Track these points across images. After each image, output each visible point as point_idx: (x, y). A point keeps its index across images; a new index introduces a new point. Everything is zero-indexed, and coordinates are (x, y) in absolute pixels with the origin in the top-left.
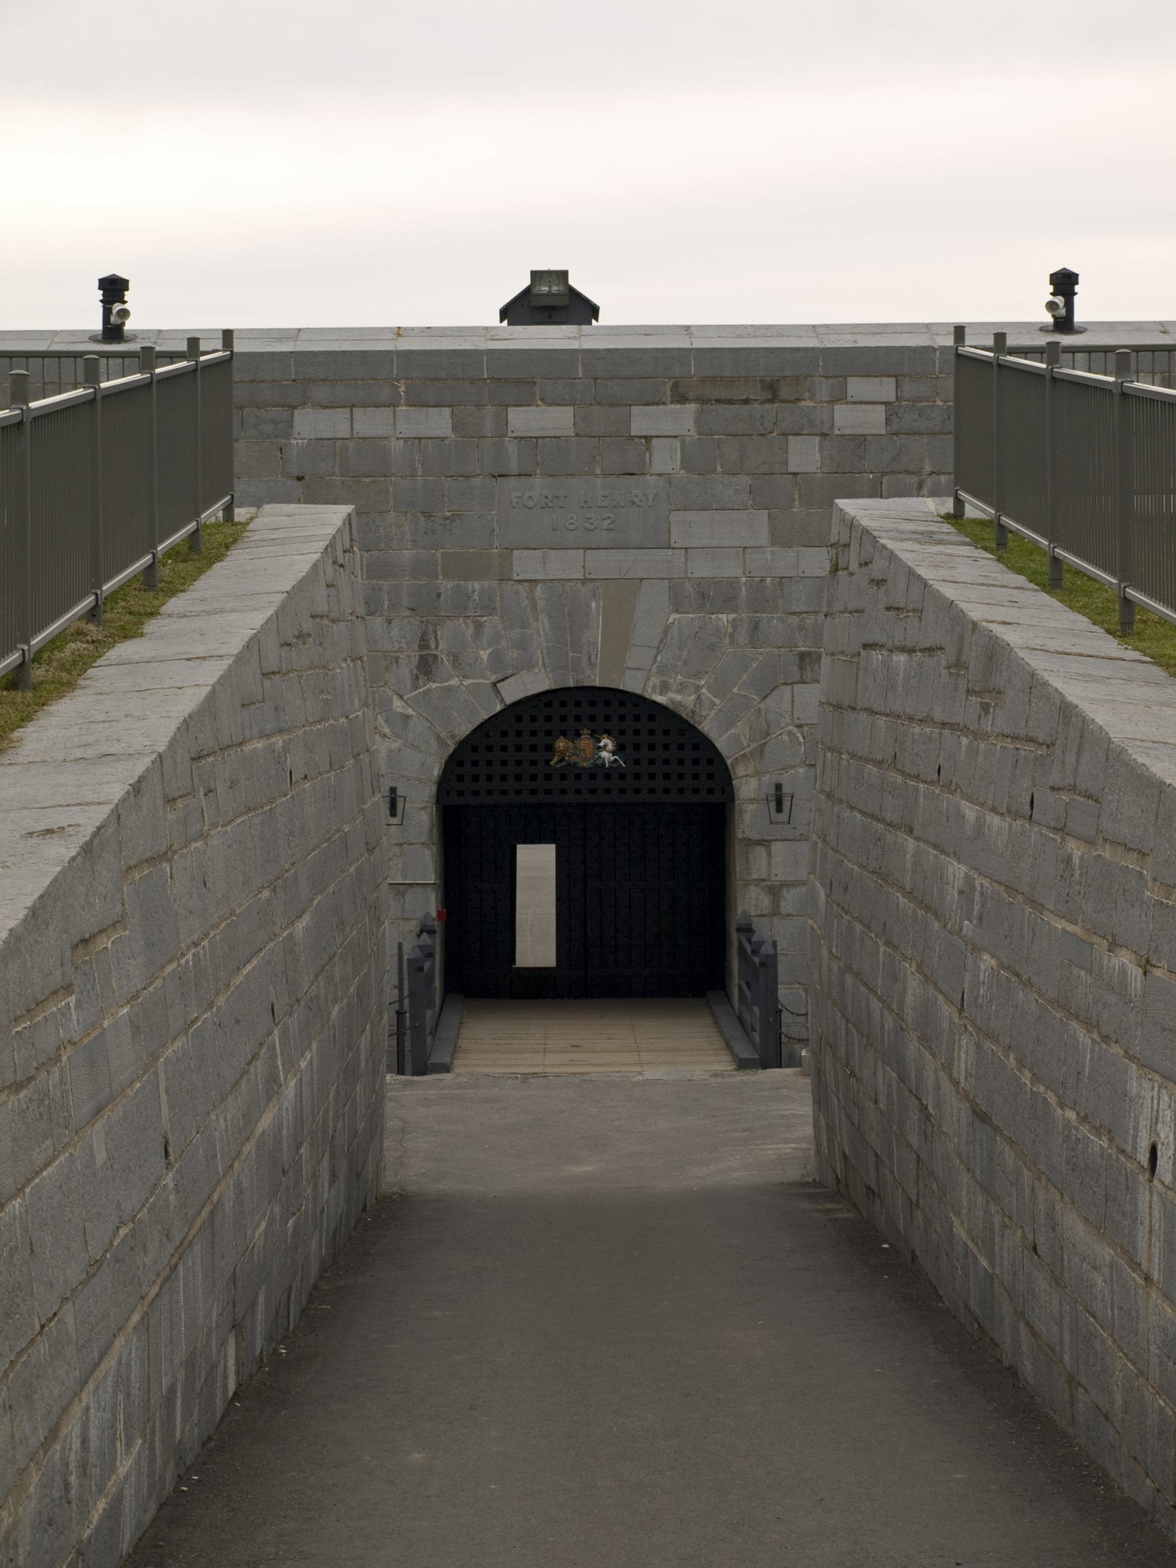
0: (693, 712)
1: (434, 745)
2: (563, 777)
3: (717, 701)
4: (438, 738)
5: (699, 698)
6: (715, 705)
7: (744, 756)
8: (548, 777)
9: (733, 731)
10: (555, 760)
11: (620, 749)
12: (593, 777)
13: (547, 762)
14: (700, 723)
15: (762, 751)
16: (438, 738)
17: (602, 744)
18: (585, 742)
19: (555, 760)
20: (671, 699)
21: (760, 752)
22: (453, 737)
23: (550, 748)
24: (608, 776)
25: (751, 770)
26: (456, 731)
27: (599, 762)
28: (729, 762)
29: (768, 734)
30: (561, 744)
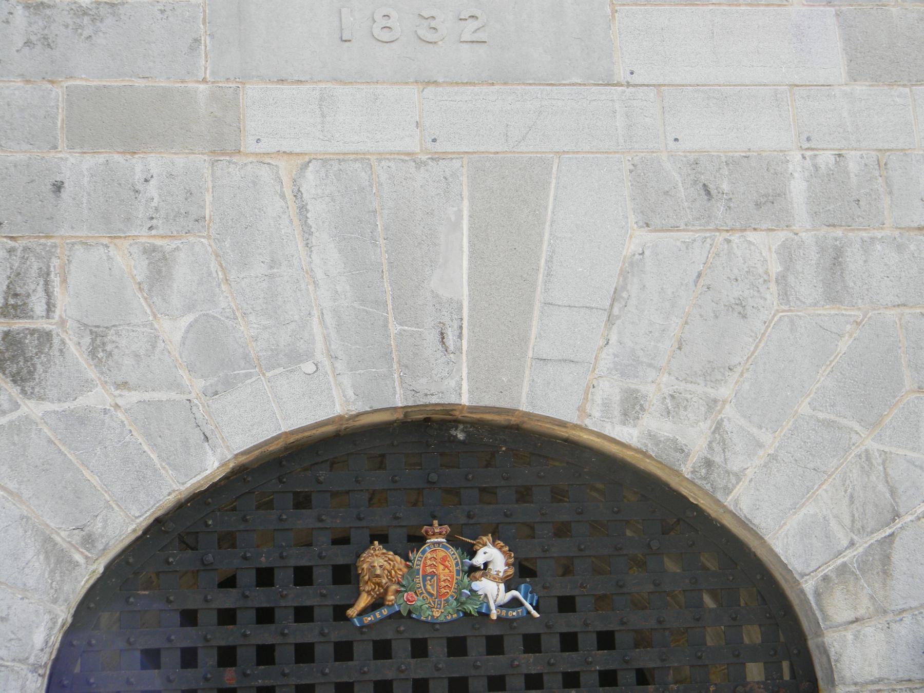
0: (708, 463)
1: (37, 567)
2: (382, 650)
3: (765, 437)
4: (47, 543)
5: (718, 427)
6: (761, 446)
7: (843, 570)
8: (344, 651)
9: (809, 509)
10: (364, 601)
11: (522, 572)
12: (457, 646)
13: (340, 613)
14: (727, 491)
15: (886, 559)
16: (47, 543)
17: (479, 560)
18: (438, 555)
19: (364, 601)
20: (652, 436)
21: (881, 559)
22: (89, 541)
23: (346, 575)
24: (495, 645)
25: (864, 607)
26: (98, 527)
27: (471, 608)
28: (808, 586)
29: (896, 515)
30: (378, 561)
